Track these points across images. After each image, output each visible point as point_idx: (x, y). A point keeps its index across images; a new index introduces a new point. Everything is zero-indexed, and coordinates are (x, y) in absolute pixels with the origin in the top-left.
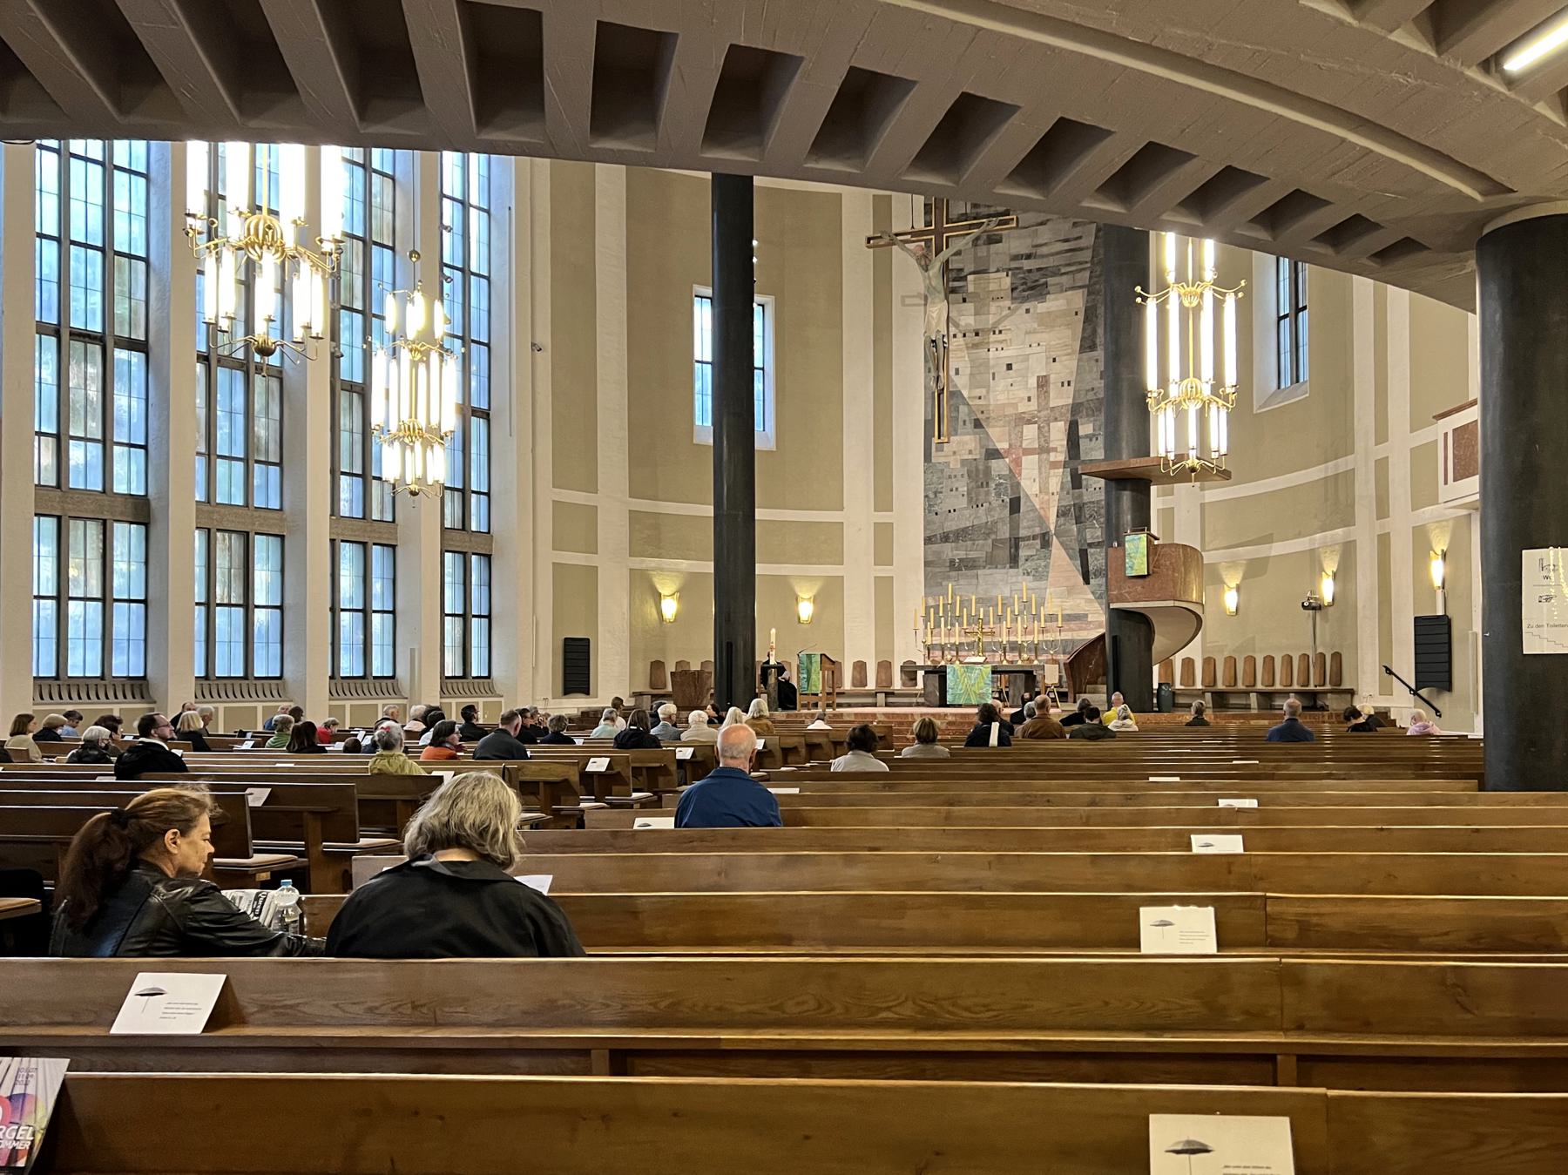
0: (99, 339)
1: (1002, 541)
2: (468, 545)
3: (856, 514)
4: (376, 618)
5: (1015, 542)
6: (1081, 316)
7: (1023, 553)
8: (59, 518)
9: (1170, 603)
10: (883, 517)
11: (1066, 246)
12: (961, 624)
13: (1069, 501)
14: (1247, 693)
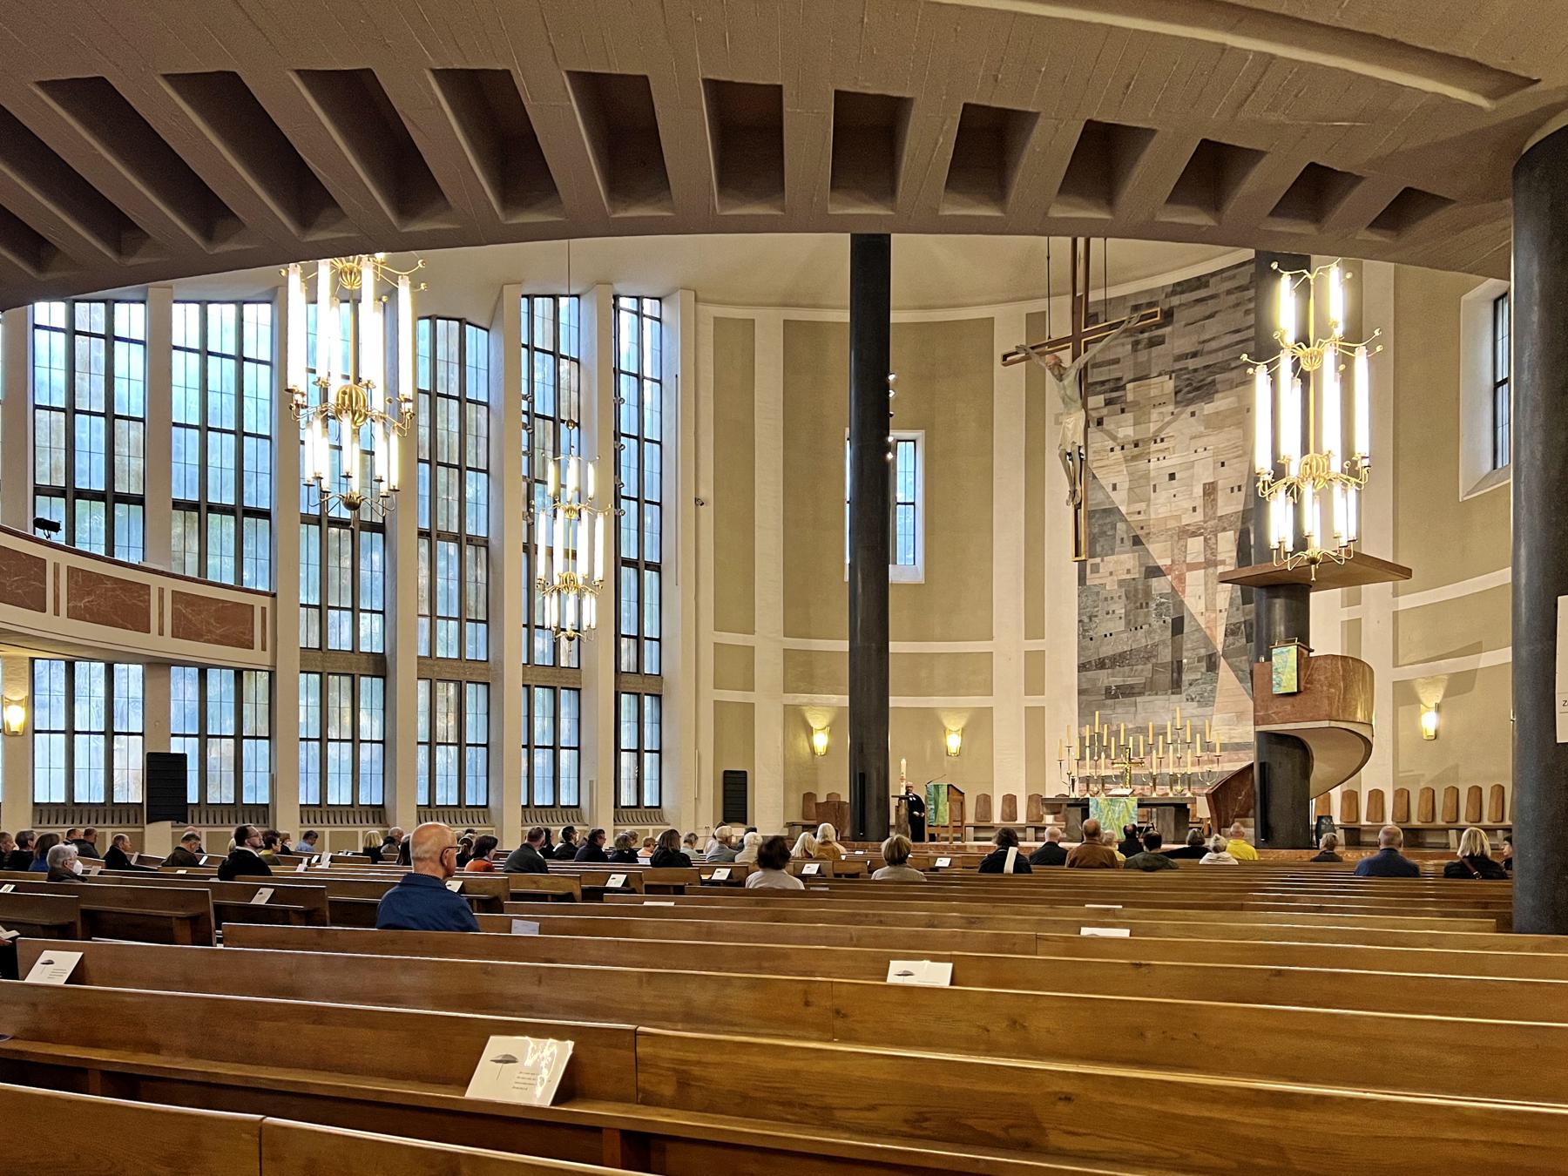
0: (194, 506)
1: (1163, 665)
2: (640, 685)
3: (1006, 643)
4: (563, 753)
7: (1186, 677)
8: (353, 676)
9: (1325, 724)
10: (1034, 645)
11: (1237, 337)
14: (1446, 830)
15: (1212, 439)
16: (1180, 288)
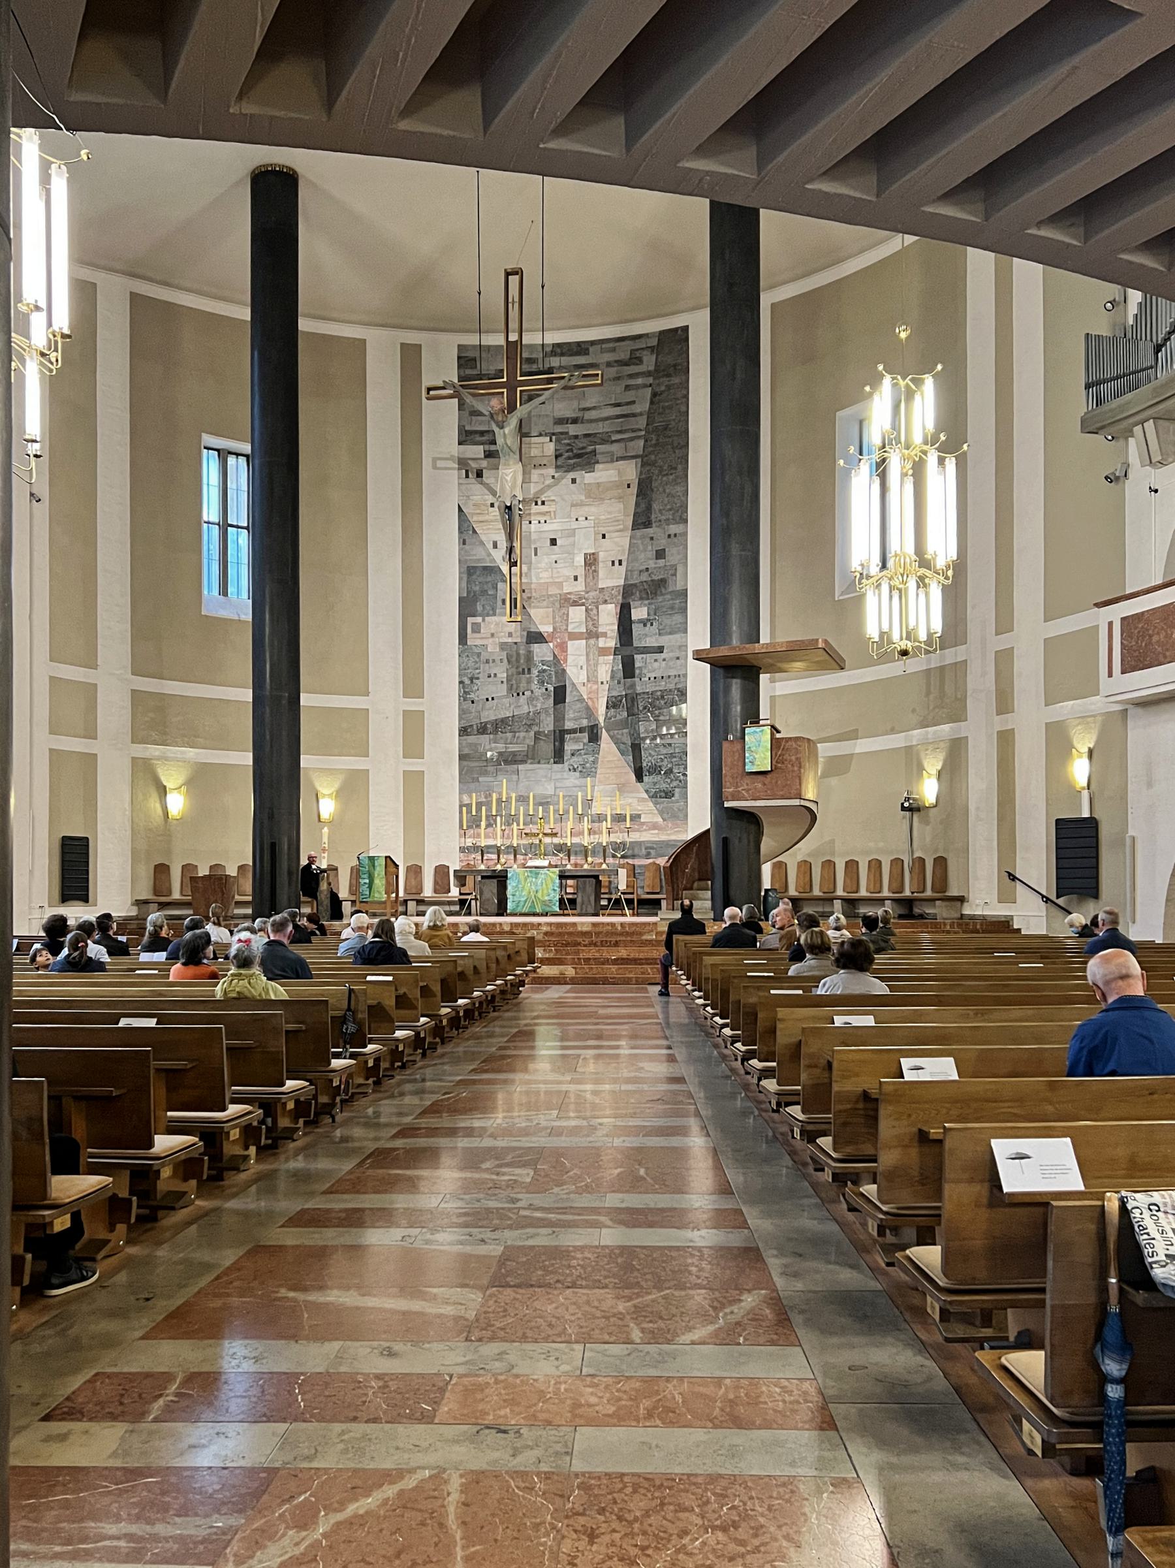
3: (384, 701)
5: (560, 736)
6: (634, 489)
7: (569, 747)
11: (618, 411)
12: (518, 825)
13: (620, 691)
15: (593, 509)
16: (560, 349)
